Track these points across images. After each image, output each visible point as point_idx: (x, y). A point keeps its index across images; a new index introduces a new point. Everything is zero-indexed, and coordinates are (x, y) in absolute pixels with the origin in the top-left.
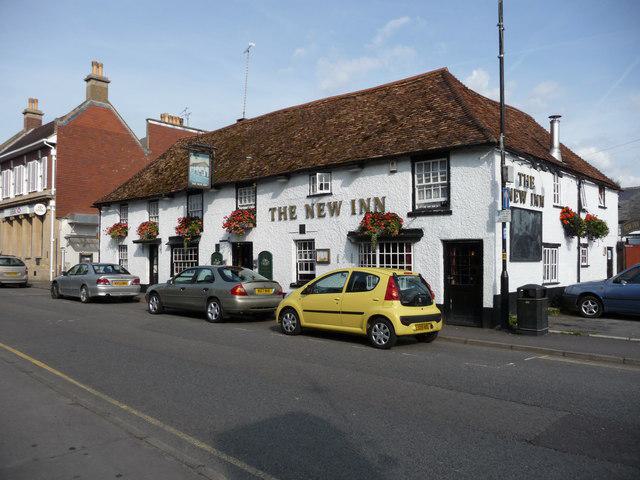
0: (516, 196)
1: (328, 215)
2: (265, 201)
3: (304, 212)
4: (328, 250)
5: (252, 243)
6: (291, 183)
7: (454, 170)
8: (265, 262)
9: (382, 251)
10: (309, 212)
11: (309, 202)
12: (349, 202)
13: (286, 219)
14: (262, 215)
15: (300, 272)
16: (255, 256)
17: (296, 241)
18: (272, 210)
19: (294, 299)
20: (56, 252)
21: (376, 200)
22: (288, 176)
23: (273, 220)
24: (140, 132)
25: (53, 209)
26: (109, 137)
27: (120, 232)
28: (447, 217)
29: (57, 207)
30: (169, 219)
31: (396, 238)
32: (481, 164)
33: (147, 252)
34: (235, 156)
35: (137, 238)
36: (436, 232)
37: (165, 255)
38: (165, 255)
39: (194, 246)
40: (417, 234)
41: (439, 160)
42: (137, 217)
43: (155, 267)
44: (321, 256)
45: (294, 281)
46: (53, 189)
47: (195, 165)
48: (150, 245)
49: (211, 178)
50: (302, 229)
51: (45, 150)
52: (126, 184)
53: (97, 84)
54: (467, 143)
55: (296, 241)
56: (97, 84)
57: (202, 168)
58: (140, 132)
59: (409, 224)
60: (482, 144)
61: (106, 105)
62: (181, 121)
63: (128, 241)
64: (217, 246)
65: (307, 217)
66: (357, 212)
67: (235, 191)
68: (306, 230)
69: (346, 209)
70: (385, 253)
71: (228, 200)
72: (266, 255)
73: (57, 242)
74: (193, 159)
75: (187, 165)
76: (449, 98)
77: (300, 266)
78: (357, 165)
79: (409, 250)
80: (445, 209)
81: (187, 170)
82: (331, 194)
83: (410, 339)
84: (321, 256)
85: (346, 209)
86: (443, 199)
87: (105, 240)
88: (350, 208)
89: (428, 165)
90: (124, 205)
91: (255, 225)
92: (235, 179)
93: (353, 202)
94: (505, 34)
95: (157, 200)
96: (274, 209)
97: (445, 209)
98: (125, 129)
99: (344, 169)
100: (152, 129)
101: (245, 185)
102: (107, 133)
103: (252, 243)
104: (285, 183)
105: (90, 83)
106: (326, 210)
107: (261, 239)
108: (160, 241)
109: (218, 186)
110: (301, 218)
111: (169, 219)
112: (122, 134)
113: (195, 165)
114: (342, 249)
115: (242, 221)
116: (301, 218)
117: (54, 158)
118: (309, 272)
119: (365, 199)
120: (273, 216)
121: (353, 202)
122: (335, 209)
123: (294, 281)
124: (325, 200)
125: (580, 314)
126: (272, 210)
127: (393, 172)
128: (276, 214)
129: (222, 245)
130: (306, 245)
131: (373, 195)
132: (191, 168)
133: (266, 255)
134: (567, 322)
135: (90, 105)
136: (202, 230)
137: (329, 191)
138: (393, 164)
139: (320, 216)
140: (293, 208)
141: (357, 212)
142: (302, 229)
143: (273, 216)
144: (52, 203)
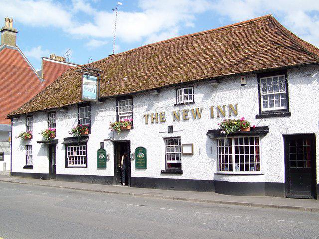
1: (191, 119)
2: (140, 110)
3: (172, 116)
4: (192, 145)
5: (129, 141)
6: (221, 86)
7: (292, 87)
8: (141, 155)
9: (237, 144)
10: (176, 117)
11: (177, 109)
12: (208, 108)
13: (157, 123)
14: (138, 121)
15: (169, 162)
16: (133, 150)
17: (165, 139)
18: (146, 116)
21: (230, 107)
23: (147, 124)
24: (38, 68)
26: (17, 70)
27: (26, 139)
30: (66, 127)
31: (248, 134)
32: (310, 82)
33: (46, 152)
34: (115, 77)
35: (41, 138)
36: (278, 128)
37: (61, 153)
38: (61, 153)
40: (264, 131)
41: (272, 77)
42: (40, 127)
43: (53, 161)
44: (186, 150)
45: (164, 168)
47: (87, 84)
48: (50, 146)
49: (98, 95)
50: (171, 129)
52: (31, 101)
54: (301, 63)
55: (165, 139)
57: (92, 86)
58: (38, 68)
59: (255, 123)
60: (313, 64)
63: (33, 142)
64: (102, 144)
65: (174, 121)
66: (215, 115)
67: (175, 91)
68: (174, 130)
69: (206, 113)
70: (239, 146)
71: (251, 89)
72: (141, 150)
74: (85, 80)
75: (81, 85)
76: (278, 34)
77: (168, 157)
78: (217, 81)
79: (257, 142)
80: (286, 113)
81: (82, 87)
82: (194, 102)
84: (186, 150)
85: (206, 113)
86: (283, 108)
87: (17, 143)
88: (209, 112)
89: (270, 80)
90: (29, 116)
91: (132, 128)
92: (116, 93)
93: (212, 108)
95: (55, 112)
96: (148, 116)
97: (286, 113)
98: (27, 64)
99: (206, 84)
100: (46, 64)
101: (126, 98)
102: (16, 68)
103: (129, 141)
104: (157, 95)
105: (4, 33)
106: (190, 114)
107: (136, 138)
108: (57, 141)
109: (103, 100)
110: (169, 120)
111: (66, 127)
112: (27, 70)
113: (87, 84)
114: (204, 143)
115: (121, 127)
116: (169, 120)
118: (176, 162)
119: (233, 105)
120: (146, 120)
121: (212, 108)
122: (197, 114)
123: (164, 168)
124: (189, 107)
126: (146, 116)
128: (149, 119)
129: (105, 143)
130: (174, 142)
131: (227, 103)
132: (84, 86)
133: (141, 150)
135: (4, 48)
136: (90, 133)
137: (192, 101)
138: (243, 79)
139: (185, 120)
140: (163, 114)
141: (215, 115)
142: (171, 129)
143: (146, 120)
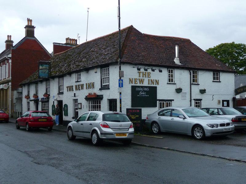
0: (79, 88)
10: (76, 89)
19: (73, 123)
20: (12, 105)
22: (70, 74)
24: (50, 49)
25: (10, 86)
28: (108, 90)
29: (12, 85)
39: (48, 101)
46: (10, 78)
51: (8, 60)
53: (30, 30)
56: (30, 30)
57: (45, 71)
58: (50, 49)
61: (33, 39)
62: (76, 41)
73: (12, 101)
79: (100, 103)
83: (117, 143)
94: (117, 14)
100: (57, 47)
117: (10, 64)
125: (152, 133)
127: (134, 67)
134: (85, 134)
144: (10, 84)
